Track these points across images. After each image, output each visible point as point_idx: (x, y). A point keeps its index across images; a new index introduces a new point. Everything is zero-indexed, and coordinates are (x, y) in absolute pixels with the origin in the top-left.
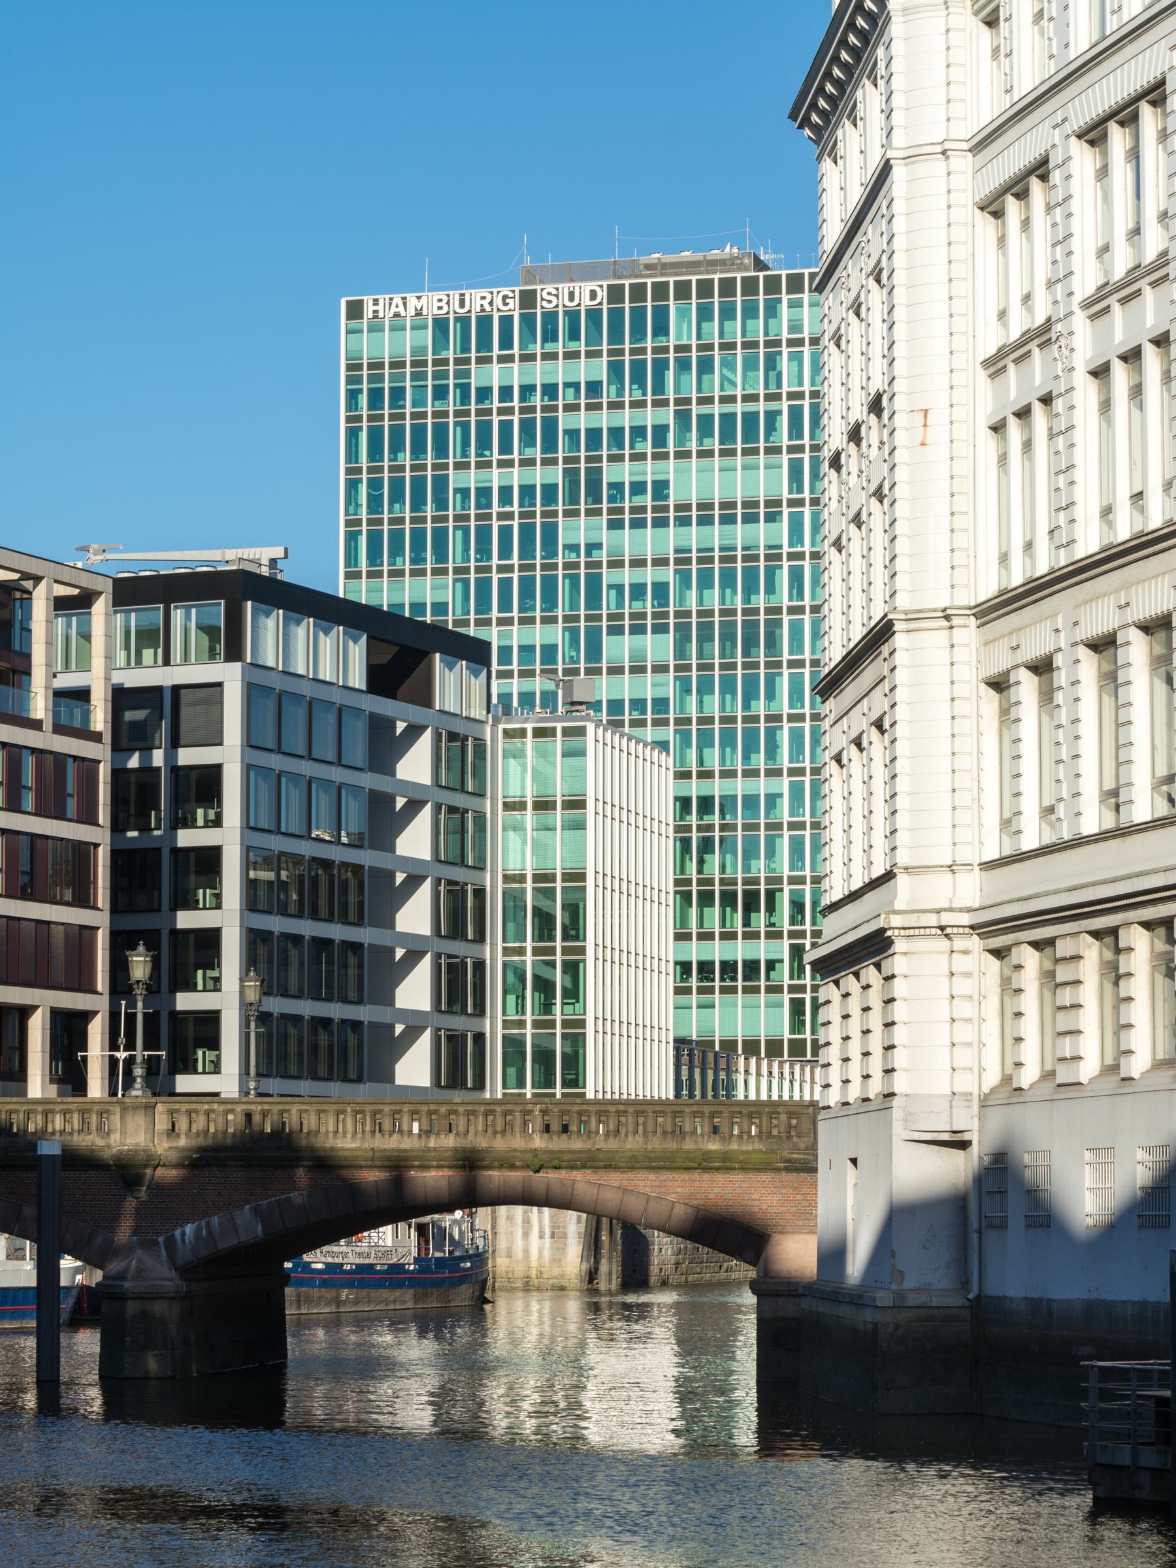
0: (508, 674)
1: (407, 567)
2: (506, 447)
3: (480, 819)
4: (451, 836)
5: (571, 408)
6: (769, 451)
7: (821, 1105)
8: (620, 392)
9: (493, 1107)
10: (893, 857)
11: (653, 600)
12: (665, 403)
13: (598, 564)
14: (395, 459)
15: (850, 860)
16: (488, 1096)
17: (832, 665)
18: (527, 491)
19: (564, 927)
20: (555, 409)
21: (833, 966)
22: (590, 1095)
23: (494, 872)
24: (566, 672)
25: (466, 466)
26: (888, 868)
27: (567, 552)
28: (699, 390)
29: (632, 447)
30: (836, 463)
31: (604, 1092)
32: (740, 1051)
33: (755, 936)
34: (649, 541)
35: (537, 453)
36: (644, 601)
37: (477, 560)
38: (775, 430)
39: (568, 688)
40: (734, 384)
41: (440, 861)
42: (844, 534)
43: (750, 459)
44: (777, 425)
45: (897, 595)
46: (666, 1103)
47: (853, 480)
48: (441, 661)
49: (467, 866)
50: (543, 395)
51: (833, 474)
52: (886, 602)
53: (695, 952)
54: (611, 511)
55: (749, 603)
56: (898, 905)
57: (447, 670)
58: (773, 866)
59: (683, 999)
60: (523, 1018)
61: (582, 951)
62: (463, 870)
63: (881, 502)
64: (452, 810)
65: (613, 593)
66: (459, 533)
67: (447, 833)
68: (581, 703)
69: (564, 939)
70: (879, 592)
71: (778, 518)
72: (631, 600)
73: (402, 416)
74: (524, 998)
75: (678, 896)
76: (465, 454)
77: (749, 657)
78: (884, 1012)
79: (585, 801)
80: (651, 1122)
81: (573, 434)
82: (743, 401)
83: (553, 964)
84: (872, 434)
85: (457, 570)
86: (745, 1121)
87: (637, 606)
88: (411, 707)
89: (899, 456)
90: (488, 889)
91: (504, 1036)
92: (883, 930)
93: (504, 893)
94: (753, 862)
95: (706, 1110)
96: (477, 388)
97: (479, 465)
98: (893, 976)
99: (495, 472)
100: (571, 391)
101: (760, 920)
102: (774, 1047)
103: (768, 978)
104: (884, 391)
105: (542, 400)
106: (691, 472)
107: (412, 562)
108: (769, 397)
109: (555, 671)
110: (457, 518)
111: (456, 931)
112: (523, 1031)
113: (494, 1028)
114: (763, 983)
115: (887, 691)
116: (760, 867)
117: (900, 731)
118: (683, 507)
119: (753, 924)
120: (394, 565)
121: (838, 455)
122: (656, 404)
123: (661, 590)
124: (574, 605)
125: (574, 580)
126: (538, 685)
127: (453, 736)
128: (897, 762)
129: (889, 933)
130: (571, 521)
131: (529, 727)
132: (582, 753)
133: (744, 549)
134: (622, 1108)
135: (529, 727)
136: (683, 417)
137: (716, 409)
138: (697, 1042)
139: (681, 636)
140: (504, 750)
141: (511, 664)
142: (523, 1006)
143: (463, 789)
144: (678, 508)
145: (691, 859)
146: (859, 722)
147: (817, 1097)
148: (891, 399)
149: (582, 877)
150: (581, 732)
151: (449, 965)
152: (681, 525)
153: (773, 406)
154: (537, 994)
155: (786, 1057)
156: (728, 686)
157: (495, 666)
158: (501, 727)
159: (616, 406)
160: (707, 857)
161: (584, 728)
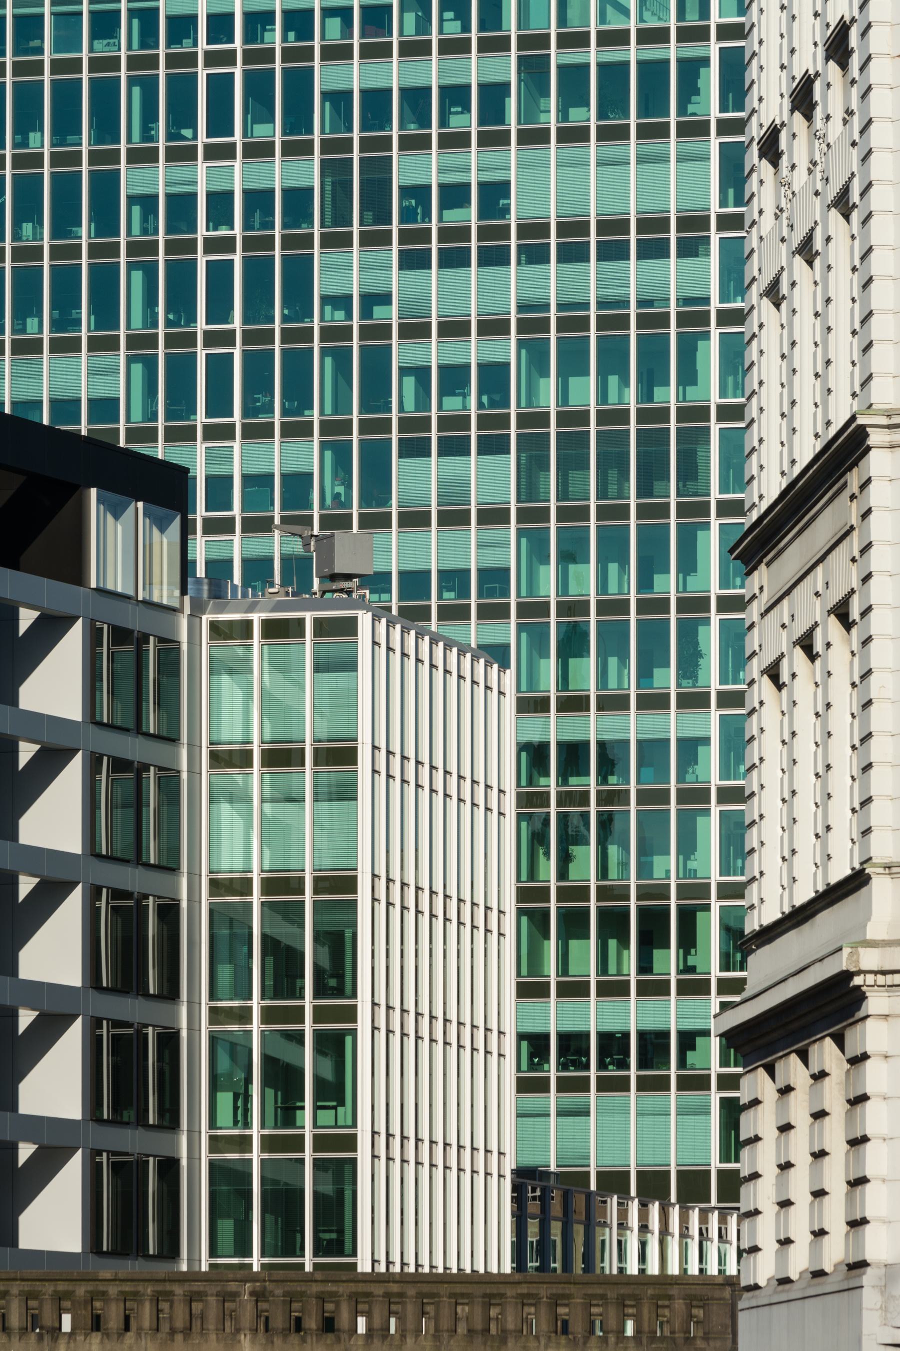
0: (224, 526)
1: (46, 336)
2: (220, 122)
3: (169, 782)
4: (119, 812)
5: (337, 53)
6: (685, 130)
7: (743, 1283)
8: (423, 25)
9: (168, 1287)
10: (865, 847)
11: (480, 394)
12: (502, 44)
13: (384, 331)
14: (25, 144)
15: (793, 852)
16: (184, 1267)
17: (764, 506)
18: (259, 201)
19: (318, 972)
20: (308, 53)
21: (763, 1040)
22: (364, 1265)
23: (194, 875)
24: (327, 522)
25: (150, 156)
26: (857, 866)
27: (328, 309)
28: (562, 21)
29: (443, 123)
30: (771, 148)
31: (389, 1263)
32: (633, 1193)
33: (659, 989)
34: (473, 290)
35: (276, 132)
36: (465, 395)
37: (168, 323)
38: (697, 92)
39: (326, 545)
40: (626, 12)
41: (99, 856)
42: (785, 275)
43: (653, 146)
44: (700, 83)
45: (873, 383)
46: (500, 1279)
47: (800, 179)
48: (99, 500)
49: (147, 865)
50: (286, 29)
51: (765, 167)
52: (854, 395)
53: (553, 1016)
54: (405, 237)
55: (650, 399)
56: (873, 932)
57: (110, 518)
58: (692, 865)
59: (533, 1100)
60: (247, 1132)
61: (350, 1014)
62: (140, 871)
63: (847, 217)
64: (120, 765)
65: (410, 382)
66: (138, 276)
67: (112, 806)
68: (349, 577)
69: (319, 992)
70: (842, 378)
71: (701, 248)
72: (442, 394)
73: (38, 67)
74: (247, 1098)
75: (524, 919)
76: (148, 134)
77: (651, 495)
78: (850, 1118)
79: (355, 749)
80: (446, 1311)
81: (339, 100)
82: (599, 44)
83: (299, 1038)
84: (832, 98)
85: (134, 341)
86: (612, 1312)
87: (453, 404)
88: (46, 583)
89: (878, 135)
90: (184, 905)
91: (212, 1164)
92: (847, 975)
93: (211, 912)
94: (657, 860)
95: (544, 1291)
96: (169, 18)
97: (173, 155)
98: (865, 1057)
99: (202, 167)
100: (335, 23)
101: (669, 962)
102: (693, 1185)
103: (682, 1063)
104: (853, 20)
105: (285, 39)
106: (548, 166)
107: (55, 325)
108: (685, 35)
109: (308, 521)
110: (134, 248)
111: (129, 980)
112: (247, 1156)
113: (194, 1149)
114: (673, 1072)
115: (856, 553)
116: (669, 868)
117: (878, 623)
118: (534, 230)
119: (656, 968)
120: (23, 331)
121: (773, 133)
122: (485, 46)
123: (494, 376)
124: (341, 402)
125: (342, 359)
126: (277, 545)
127: (120, 635)
128: (873, 678)
129: (857, 981)
130: (336, 255)
131: (256, 618)
132: (350, 665)
133: (640, 303)
134: (395, 1288)
135: (256, 618)
136: (533, 69)
137: (593, 56)
138: (556, 1174)
139: (530, 458)
140: (211, 659)
141: (230, 508)
142: (247, 1111)
143: (139, 729)
144: (525, 230)
145: (547, 854)
146: (808, 608)
147: (732, 1269)
148: (864, 34)
149: (349, 884)
150: (349, 627)
151: (115, 1040)
152: (531, 261)
153: (693, 50)
154: (270, 1092)
155: (714, 1202)
156: (613, 548)
157: (201, 512)
158: (206, 618)
159: (415, 49)
160: (575, 850)
161: (355, 619)
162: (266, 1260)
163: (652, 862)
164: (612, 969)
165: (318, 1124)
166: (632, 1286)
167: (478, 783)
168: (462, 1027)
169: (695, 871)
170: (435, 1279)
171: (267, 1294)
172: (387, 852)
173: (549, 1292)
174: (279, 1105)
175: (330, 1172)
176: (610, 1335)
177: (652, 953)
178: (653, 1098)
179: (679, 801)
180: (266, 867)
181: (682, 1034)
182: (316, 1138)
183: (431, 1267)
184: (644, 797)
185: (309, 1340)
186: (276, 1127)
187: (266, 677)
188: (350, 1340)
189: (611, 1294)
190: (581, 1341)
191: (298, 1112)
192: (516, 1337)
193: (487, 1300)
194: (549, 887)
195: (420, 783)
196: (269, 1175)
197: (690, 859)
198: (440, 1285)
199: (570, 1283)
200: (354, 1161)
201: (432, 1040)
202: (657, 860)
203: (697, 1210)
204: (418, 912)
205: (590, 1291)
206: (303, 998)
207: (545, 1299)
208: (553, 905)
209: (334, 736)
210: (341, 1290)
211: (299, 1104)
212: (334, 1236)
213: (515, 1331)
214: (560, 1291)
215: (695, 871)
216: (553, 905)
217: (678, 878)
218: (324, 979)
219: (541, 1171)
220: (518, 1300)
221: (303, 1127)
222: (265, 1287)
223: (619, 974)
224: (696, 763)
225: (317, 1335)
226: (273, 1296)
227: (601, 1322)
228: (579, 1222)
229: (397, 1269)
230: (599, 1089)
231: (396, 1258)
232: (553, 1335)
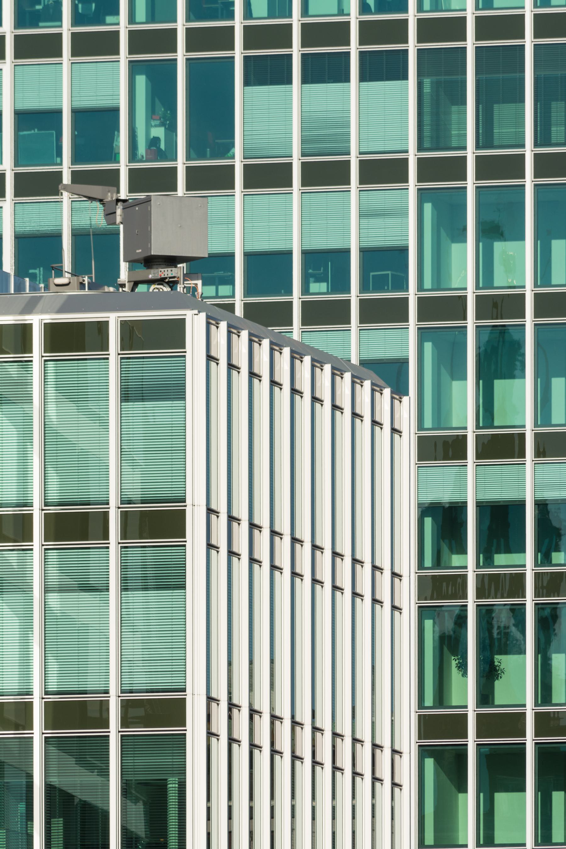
145: (463, 667)
149: (175, 711)
167: (216, 513)
208: (471, 741)
209: (151, 494)
216: (471, 741)
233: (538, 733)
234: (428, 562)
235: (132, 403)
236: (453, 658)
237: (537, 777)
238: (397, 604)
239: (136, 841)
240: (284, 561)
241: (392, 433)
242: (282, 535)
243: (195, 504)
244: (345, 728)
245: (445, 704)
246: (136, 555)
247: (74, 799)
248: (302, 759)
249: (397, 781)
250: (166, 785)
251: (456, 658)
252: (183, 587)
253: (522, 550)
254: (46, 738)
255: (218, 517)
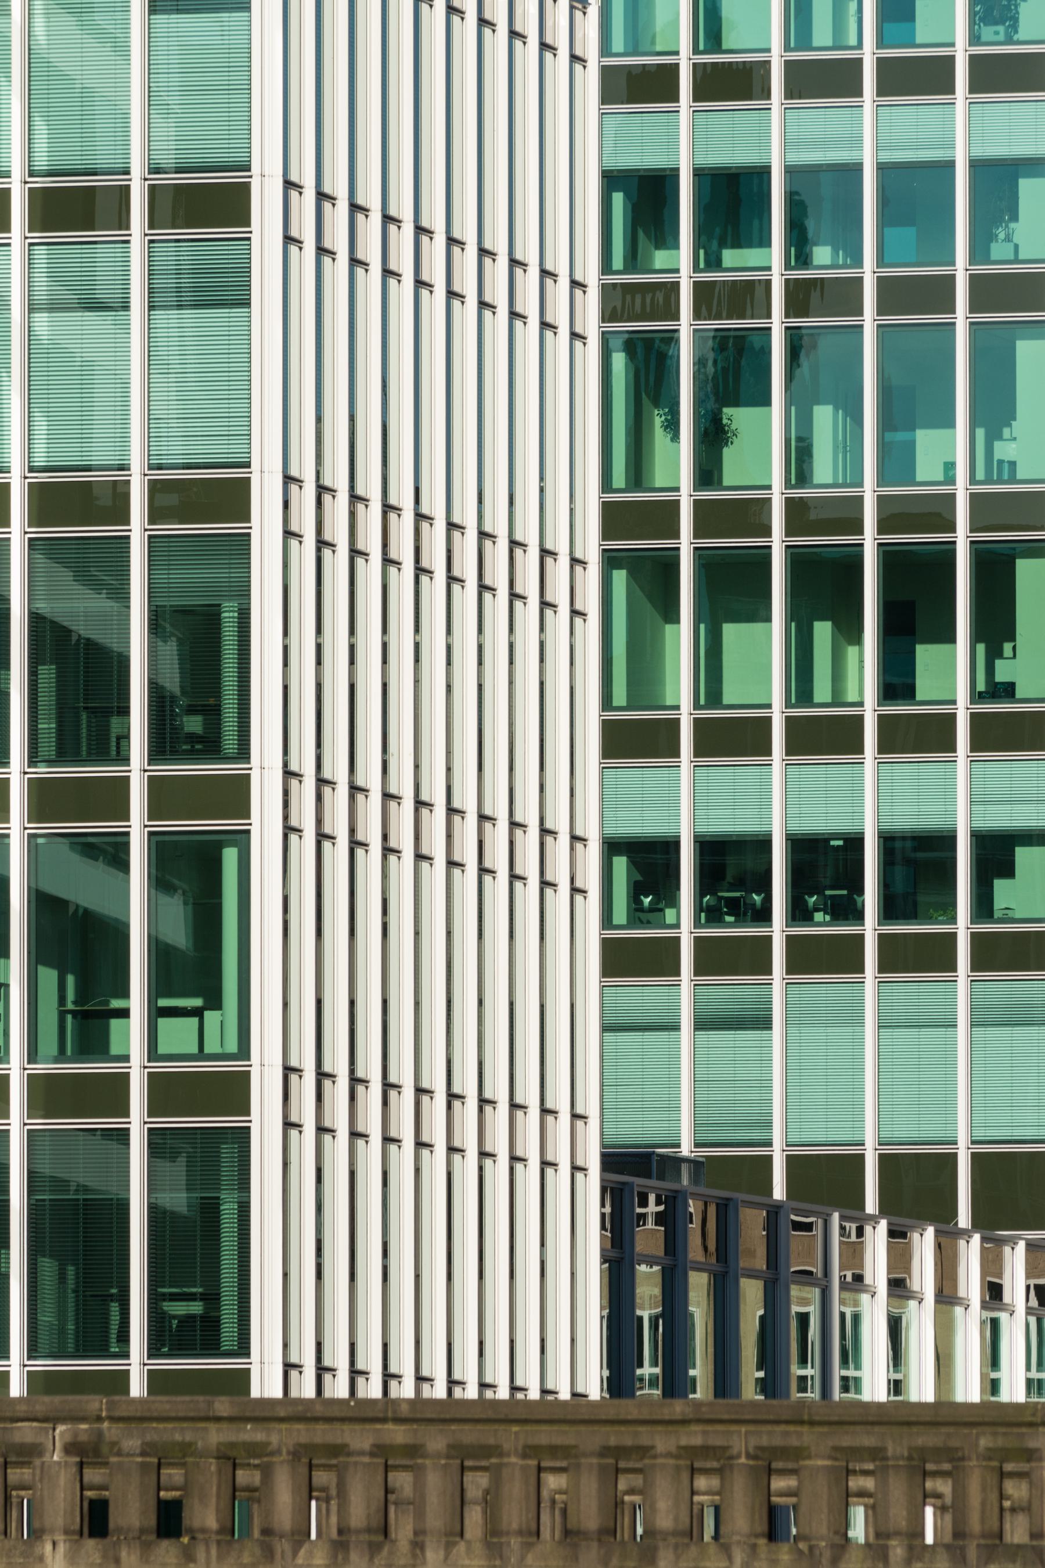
31: (388, 1376)
32: (871, 1205)
46: (575, 1413)
58: (1004, 450)
59: (641, 994)
61: (235, 797)
79: (244, 190)
83: (114, 851)
86: (898, 1489)
94: (925, 439)
95: (741, 1442)
101: (951, 673)
103: (983, 905)
114: (963, 926)
134: (398, 1434)
138: (696, 1165)
145: (673, 426)
149: (231, 498)
154: (48, 976)
160: (738, 417)
162: (42, 1365)
163: (913, 443)
164: (822, 691)
165: (161, 1050)
166: (944, 1430)
167: (461, 243)
168: (457, 818)
169: (1013, 464)
170: (490, 1414)
171: (105, 1450)
172: (319, 419)
173: (753, 1442)
174: (70, 1006)
175: (182, 1160)
176: (893, 1543)
177: (913, 652)
178: (916, 990)
179: (976, 305)
180: (40, 461)
181: (981, 840)
182: (157, 1083)
183: (483, 1386)
184: (894, 295)
185: (201, 1554)
186: (61, 1056)
187: (39, 22)
188: (295, 1553)
189: (896, 1447)
190: (827, 1554)
191: (114, 1023)
192: (676, 1547)
193: (611, 1461)
194: (677, 503)
195: (519, 309)
196: (45, 1169)
197: (1000, 438)
198: (502, 1427)
199: (802, 1423)
200: (243, 1135)
201: (420, 857)
202: (925, 439)
203: (1022, 1245)
204: (355, 553)
205: (846, 1441)
206: (126, 760)
207: (743, 1460)
208: (686, 544)
209: (195, 158)
210: (274, 1439)
211: (116, 1004)
212: (196, 1308)
213: (675, 1533)
214: (778, 1442)
215: (1013, 464)
216: (686, 544)
217: (973, 480)
218: (173, 716)
219: (662, 1156)
220: (682, 1462)
221: (126, 1058)
222: (100, 1434)
223: (837, 701)
224: (1015, 218)
225: (219, 1542)
226: (119, 1454)
227: (717, 1509)
228: (752, 1275)
229: (406, 1390)
230: (793, 966)
231: (371, 1361)
232: (762, 1542)
233: (789, 531)
234: (618, 263)
235: (166, 16)
236: (656, 412)
237: (789, 599)
238: (549, 319)
239: (171, 702)
240: (371, 252)
241: (571, 62)
242: (400, 222)
243: (266, 174)
244: (529, 534)
245: (645, 485)
246: (167, 254)
247: (71, 636)
248: (585, 615)
249: (549, 598)
250: (220, 615)
251: (661, 412)
252: (246, 303)
253: (765, 241)
254: (30, 539)
255: (301, 193)
